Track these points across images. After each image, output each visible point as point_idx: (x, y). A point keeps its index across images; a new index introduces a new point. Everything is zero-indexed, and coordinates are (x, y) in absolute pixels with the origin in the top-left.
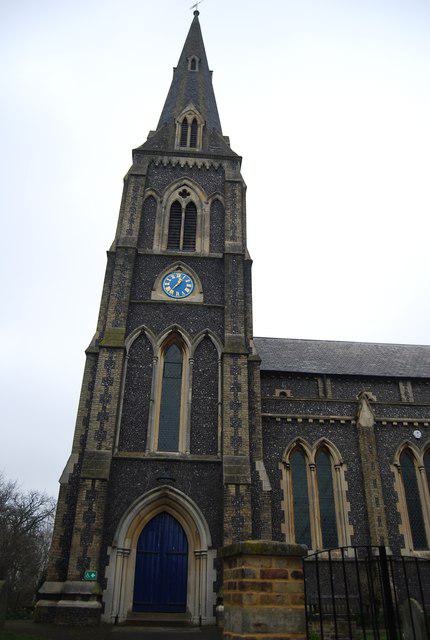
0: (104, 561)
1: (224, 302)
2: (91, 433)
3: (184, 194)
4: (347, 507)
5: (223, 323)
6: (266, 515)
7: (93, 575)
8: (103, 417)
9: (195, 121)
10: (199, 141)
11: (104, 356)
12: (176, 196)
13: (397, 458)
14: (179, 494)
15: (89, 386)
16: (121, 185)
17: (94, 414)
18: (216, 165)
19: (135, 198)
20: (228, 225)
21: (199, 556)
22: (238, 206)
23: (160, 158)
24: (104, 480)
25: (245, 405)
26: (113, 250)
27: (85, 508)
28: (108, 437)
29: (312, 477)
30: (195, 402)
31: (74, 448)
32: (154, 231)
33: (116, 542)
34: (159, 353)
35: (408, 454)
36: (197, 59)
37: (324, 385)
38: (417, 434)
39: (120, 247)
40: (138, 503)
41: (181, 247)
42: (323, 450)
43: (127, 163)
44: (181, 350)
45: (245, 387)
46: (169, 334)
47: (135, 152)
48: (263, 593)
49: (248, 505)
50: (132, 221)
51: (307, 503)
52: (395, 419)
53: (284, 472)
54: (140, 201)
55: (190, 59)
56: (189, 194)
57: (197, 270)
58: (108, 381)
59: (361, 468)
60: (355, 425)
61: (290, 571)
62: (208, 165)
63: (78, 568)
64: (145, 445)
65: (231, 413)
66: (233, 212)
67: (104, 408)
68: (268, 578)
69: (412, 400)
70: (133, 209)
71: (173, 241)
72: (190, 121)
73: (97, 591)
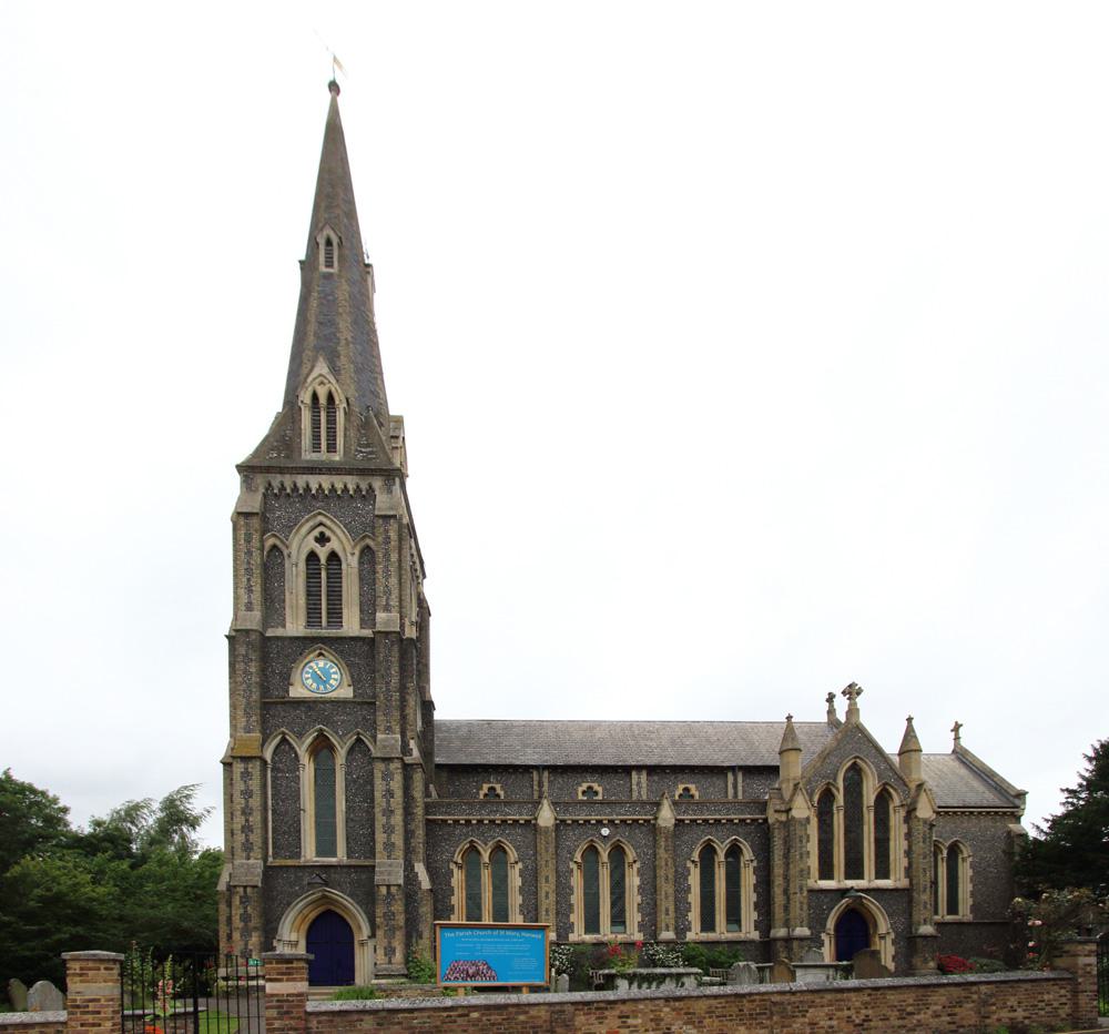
1: (375, 696)
3: (322, 539)
4: (519, 900)
9: (330, 398)
11: (239, 767)
12: (311, 544)
13: (578, 857)
16: (231, 524)
18: (364, 486)
19: (249, 553)
20: (380, 588)
30: (349, 809)
32: (284, 601)
33: (281, 935)
34: (305, 758)
35: (592, 850)
36: (335, 241)
37: (540, 777)
38: (605, 832)
42: (499, 850)
43: (230, 490)
45: (399, 794)
46: (315, 739)
50: (250, 590)
52: (582, 818)
53: (455, 870)
54: (257, 559)
56: (328, 540)
57: (341, 653)
60: (654, 825)
64: (300, 852)
65: (384, 820)
66: (386, 567)
67: (247, 821)
69: (644, 797)
70: (249, 571)
72: (323, 400)
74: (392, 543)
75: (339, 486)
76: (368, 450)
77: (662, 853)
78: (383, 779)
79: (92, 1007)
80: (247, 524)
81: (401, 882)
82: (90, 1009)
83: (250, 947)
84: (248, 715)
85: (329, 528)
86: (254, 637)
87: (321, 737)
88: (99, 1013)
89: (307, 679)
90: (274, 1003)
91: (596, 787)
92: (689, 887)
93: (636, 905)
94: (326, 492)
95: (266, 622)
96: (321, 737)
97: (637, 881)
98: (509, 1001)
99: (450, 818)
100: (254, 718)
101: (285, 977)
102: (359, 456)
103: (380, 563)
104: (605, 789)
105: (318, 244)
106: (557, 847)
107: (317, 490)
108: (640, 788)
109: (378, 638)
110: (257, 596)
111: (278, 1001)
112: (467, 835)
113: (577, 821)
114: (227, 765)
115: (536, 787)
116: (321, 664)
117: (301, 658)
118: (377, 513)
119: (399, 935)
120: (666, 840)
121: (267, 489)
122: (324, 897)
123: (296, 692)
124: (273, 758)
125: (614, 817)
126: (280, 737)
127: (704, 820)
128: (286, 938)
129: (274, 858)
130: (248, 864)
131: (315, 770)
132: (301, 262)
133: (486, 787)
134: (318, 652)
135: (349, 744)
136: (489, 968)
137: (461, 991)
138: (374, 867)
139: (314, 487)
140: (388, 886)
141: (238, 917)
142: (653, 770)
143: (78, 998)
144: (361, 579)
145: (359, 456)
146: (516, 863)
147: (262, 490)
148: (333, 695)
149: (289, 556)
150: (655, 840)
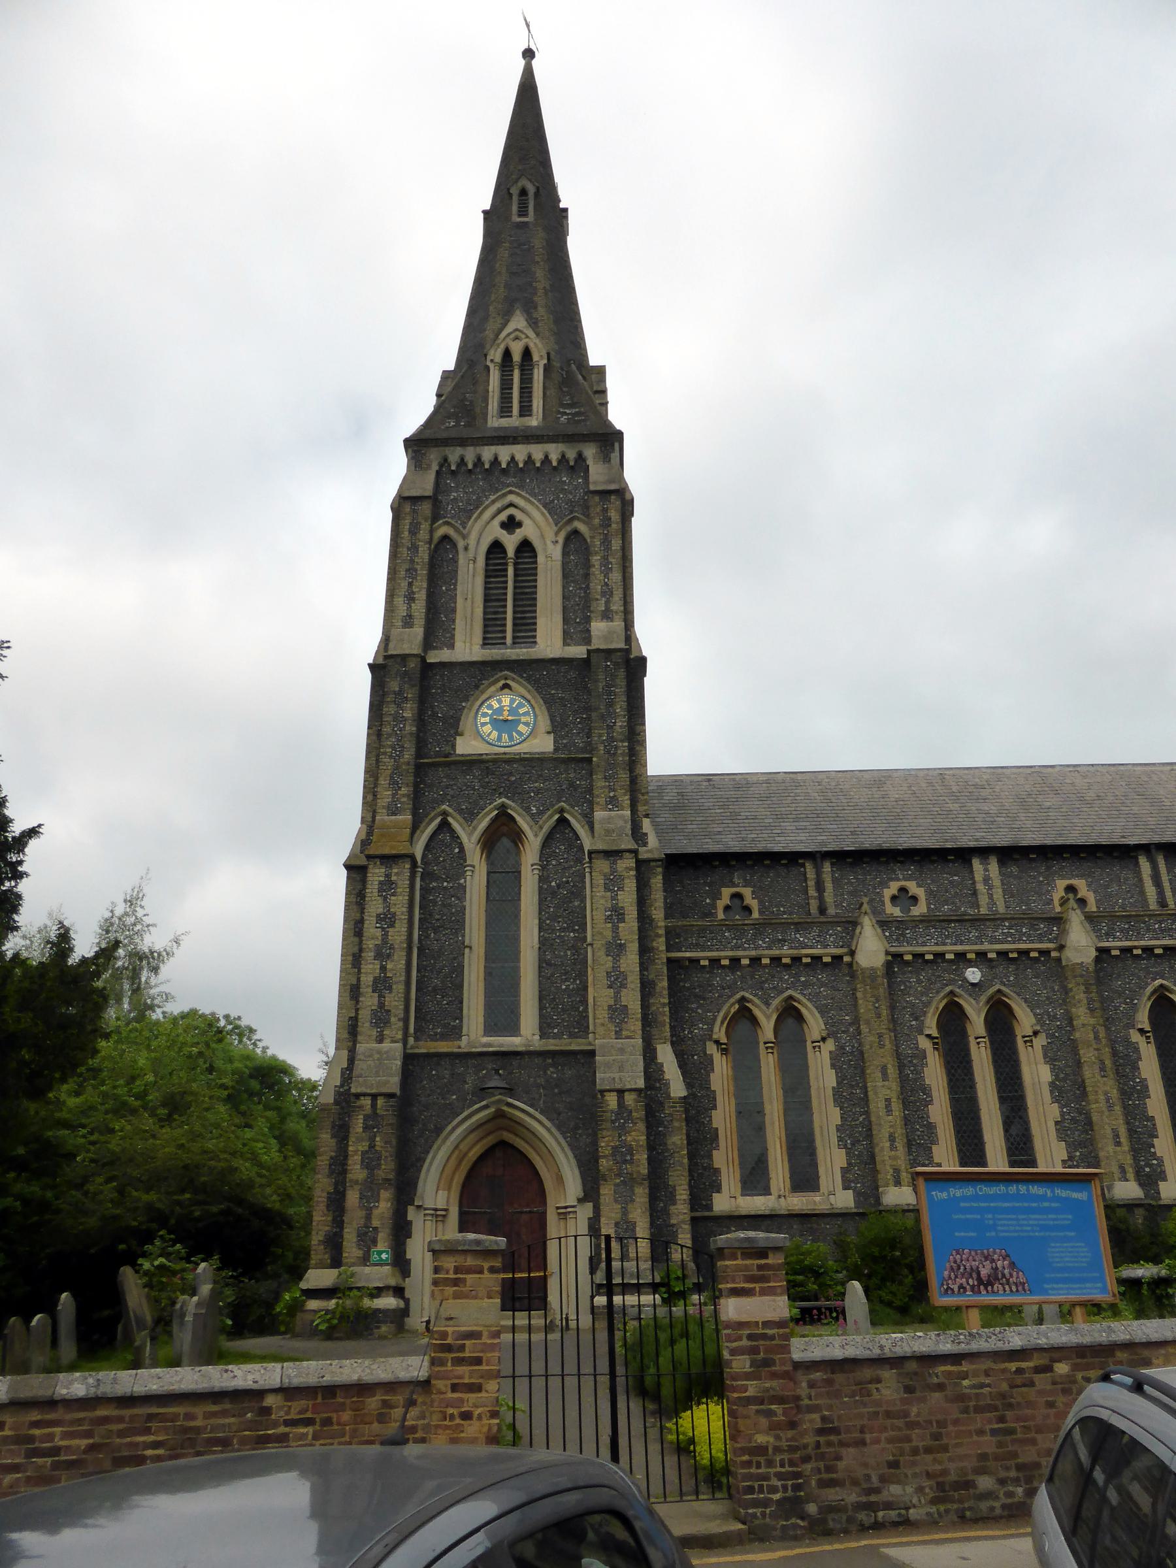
0: (401, 1231)
1: (590, 748)
2: (365, 1015)
3: (511, 524)
4: (835, 1116)
5: (590, 790)
6: (677, 1140)
7: (384, 1256)
8: (382, 984)
9: (527, 353)
10: (537, 403)
11: (376, 874)
12: (495, 531)
14: (523, 1111)
15: (355, 927)
16: (388, 516)
17: (367, 980)
18: (571, 455)
19: (414, 548)
20: (596, 587)
21: (564, 1214)
22: (616, 544)
23: (459, 451)
24: (391, 1096)
25: (634, 947)
26: (381, 661)
27: (364, 1146)
28: (393, 1019)
29: (769, 1065)
31: (338, 1040)
32: (454, 610)
35: (953, 1017)
36: (531, 189)
37: (819, 874)
38: (973, 975)
39: (392, 656)
40: (454, 1129)
41: (509, 640)
44: (517, 845)
45: (632, 913)
46: (494, 821)
47: (408, 443)
48: (455, 1288)
49: (641, 1126)
50: (410, 598)
51: (761, 1112)
52: (929, 949)
54: (424, 554)
55: (515, 191)
56: (519, 525)
58: (387, 920)
59: (860, 1044)
60: (850, 965)
61: (486, 1265)
62: (554, 458)
63: (359, 1247)
65: (608, 963)
66: (605, 558)
67: (383, 969)
68: (462, 1273)
70: (412, 572)
71: (492, 629)
72: (517, 357)
73: (392, 1282)
74: (614, 526)
75: (521, 458)
76: (574, 411)
77: (1082, 1015)
78: (607, 889)
79: (470, 1349)
80: (414, 511)
81: (641, 1083)
82: (467, 1354)
83: (375, 1223)
84: (395, 785)
85: (522, 510)
86: (412, 665)
87: (504, 819)
88: (478, 1361)
89: (483, 724)
90: (745, 1342)
91: (913, 888)
92: (1144, 1084)
93: (1051, 1124)
94: (521, 465)
95: (429, 642)
96: (504, 819)
97: (1045, 1074)
98: (1114, 1338)
99: (704, 956)
100: (404, 790)
101: (757, 1286)
102: (563, 419)
103: (596, 553)
104: (930, 894)
105: (510, 195)
106: (892, 1008)
107: (508, 464)
108: (990, 888)
109: (594, 660)
110: (419, 608)
111: (750, 1337)
112: (733, 988)
113: (922, 955)
114: (356, 870)
115: (812, 892)
116: (506, 700)
117: (477, 692)
118: (592, 488)
119: (641, 1194)
120: (1087, 991)
121: (441, 466)
122: (500, 1115)
123: (466, 746)
124: (424, 856)
125: (986, 946)
126: (439, 820)
127: (1146, 949)
128: (429, 1203)
129: (417, 1039)
130: (379, 1052)
131: (489, 873)
132: (485, 212)
133: (726, 892)
134: (503, 682)
135: (546, 828)
136: (1012, 1265)
137: (974, 1316)
138: (592, 1053)
139: (504, 461)
140: (621, 1092)
141: (358, 1158)
142: (1008, 854)
143: (450, 1330)
144: (565, 576)
145: (563, 419)
146: (824, 1039)
147: (435, 467)
148: (524, 748)
149: (466, 548)
150: (1066, 991)
